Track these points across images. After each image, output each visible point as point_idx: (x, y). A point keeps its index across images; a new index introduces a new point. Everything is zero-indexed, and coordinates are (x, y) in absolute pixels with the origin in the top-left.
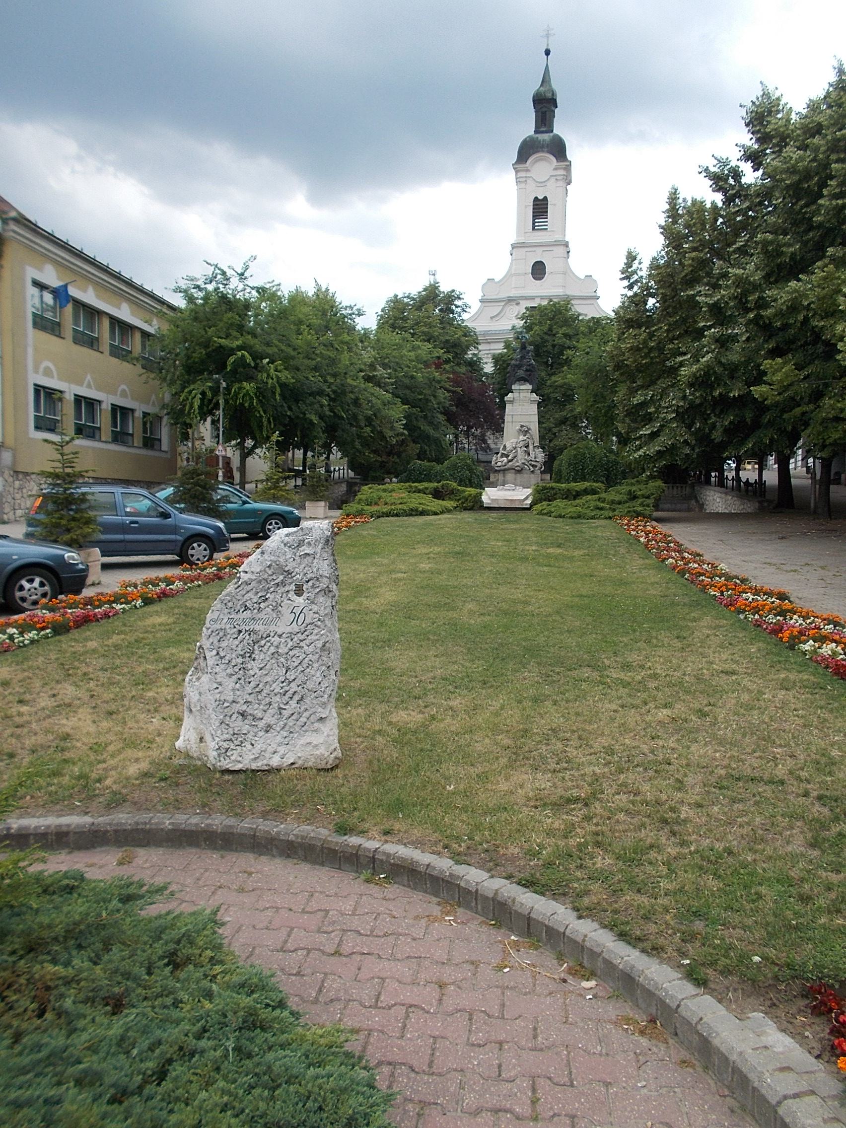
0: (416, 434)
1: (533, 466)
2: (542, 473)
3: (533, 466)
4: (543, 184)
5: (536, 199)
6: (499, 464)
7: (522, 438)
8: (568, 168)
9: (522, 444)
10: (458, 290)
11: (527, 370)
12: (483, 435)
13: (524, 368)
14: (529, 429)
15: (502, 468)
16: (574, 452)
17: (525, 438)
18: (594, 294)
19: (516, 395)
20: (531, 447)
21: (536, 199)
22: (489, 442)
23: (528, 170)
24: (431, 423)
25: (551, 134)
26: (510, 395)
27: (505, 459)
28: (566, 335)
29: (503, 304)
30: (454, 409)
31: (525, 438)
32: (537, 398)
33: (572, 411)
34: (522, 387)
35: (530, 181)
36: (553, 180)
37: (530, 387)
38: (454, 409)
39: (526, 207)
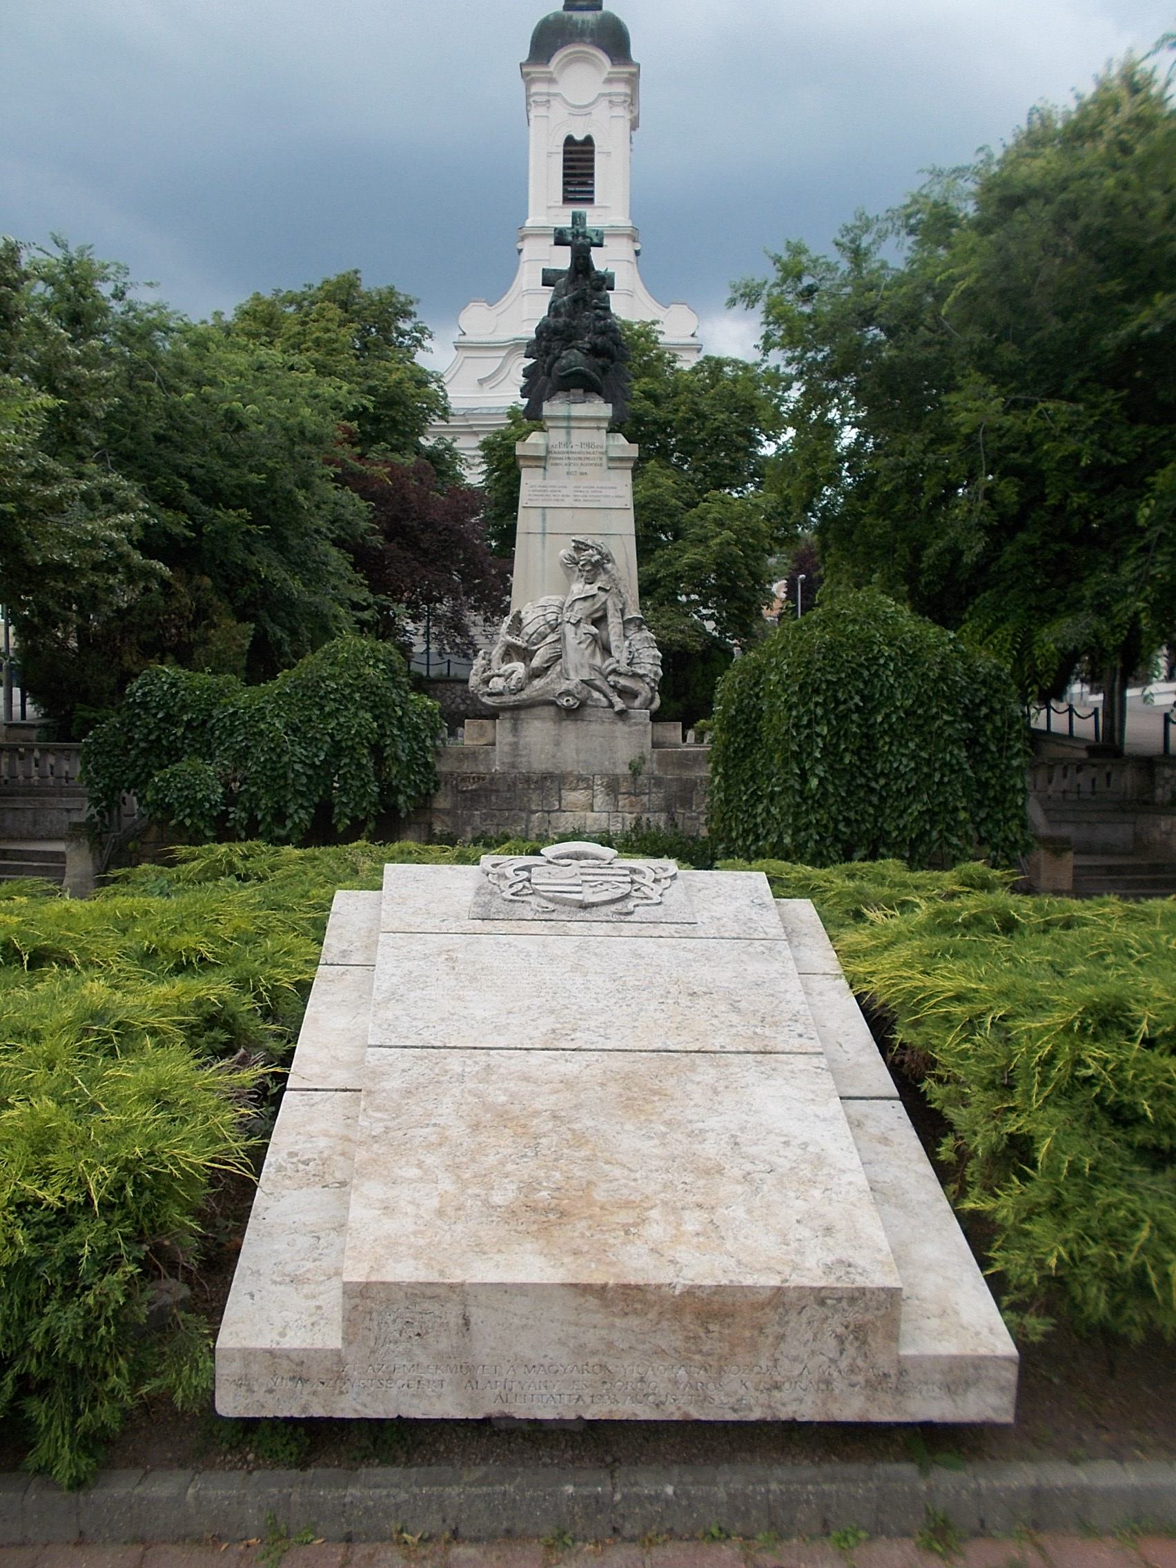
0: (244, 592)
1: (624, 693)
2: (656, 717)
3: (624, 693)
4: (583, 110)
5: (569, 141)
6: (497, 684)
7: (579, 588)
8: (633, 80)
9: (581, 610)
10: (404, 290)
11: (595, 351)
12: (457, 613)
13: (585, 342)
14: (606, 558)
15: (509, 699)
16: (823, 637)
17: (592, 589)
18: (693, 340)
19: (556, 437)
20: (614, 622)
21: (569, 141)
22: (474, 631)
23: (551, 80)
24: (297, 566)
25: (599, 13)
26: (535, 438)
27: (519, 668)
28: (649, 395)
29: (503, 353)
30: (378, 541)
31: (592, 589)
32: (633, 450)
33: (668, 563)
34: (579, 410)
35: (555, 103)
36: (604, 103)
37: (606, 410)
38: (378, 541)
39: (550, 154)
